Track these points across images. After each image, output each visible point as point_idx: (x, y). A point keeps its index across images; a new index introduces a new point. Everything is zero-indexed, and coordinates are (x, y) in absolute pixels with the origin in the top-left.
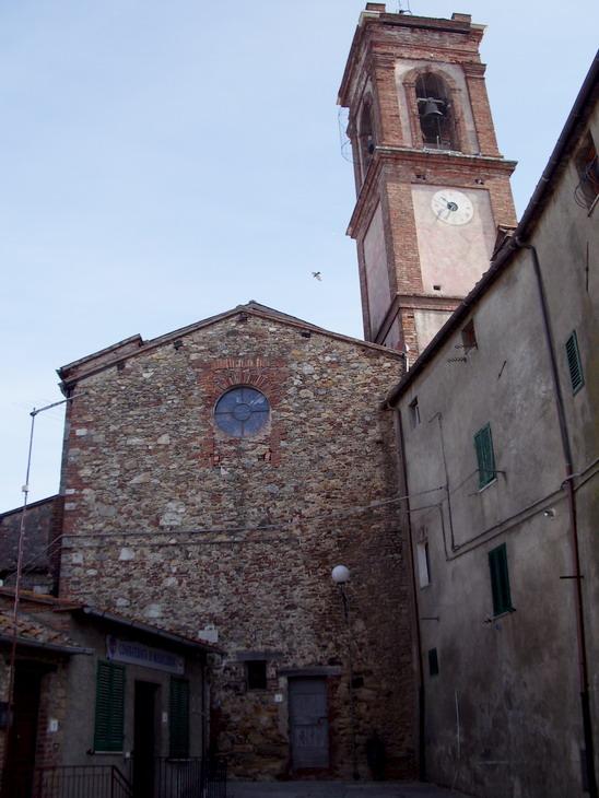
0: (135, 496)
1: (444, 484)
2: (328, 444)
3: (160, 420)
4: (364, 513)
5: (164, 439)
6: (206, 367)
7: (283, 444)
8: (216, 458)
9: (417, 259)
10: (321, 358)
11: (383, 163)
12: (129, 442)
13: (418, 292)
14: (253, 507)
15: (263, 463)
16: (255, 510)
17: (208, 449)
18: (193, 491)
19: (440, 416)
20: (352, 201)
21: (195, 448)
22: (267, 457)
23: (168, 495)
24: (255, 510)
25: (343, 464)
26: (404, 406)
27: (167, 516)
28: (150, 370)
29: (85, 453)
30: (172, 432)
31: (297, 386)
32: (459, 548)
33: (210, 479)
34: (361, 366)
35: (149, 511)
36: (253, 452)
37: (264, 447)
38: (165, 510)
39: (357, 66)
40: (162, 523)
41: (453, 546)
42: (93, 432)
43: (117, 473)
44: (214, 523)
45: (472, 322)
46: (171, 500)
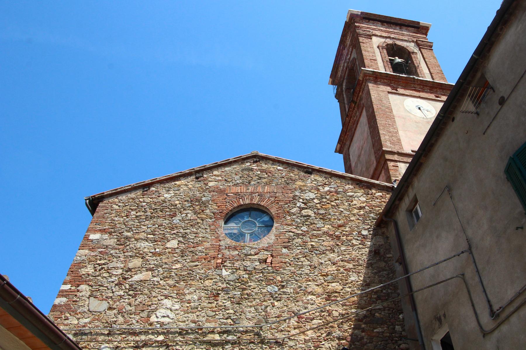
0: (131, 293)
1: (464, 246)
2: (327, 252)
3: (172, 229)
4: (365, 316)
5: (173, 244)
6: (221, 192)
7: (284, 251)
8: (220, 261)
9: (397, 133)
10: (320, 188)
11: (366, 80)
12: (138, 245)
13: (400, 151)
14: (251, 306)
15: (265, 266)
16: (252, 309)
17: (212, 253)
18: (191, 290)
19: (449, 189)
20: (339, 127)
21: (201, 252)
22: (269, 261)
23: (166, 292)
24: (252, 309)
25: (342, 269)
26: (401, 216)
27: (161, 312)
28: (171, 192)
29: (93, 254)
30: (181, 239)
31: (299, 207)
32: (503, 309)
33: (211, 279)
34: (356, 194)
35: (142, 308)
36: (256, 257)
37: (266, 253)
38: (159, 305)
39: (344, 51)
40: (153, 319)
41: (492, 313)
42: (106, 236)
43: (120, 271)
44: (207, 321)
45: (483, 76)
46: (166, 297)
